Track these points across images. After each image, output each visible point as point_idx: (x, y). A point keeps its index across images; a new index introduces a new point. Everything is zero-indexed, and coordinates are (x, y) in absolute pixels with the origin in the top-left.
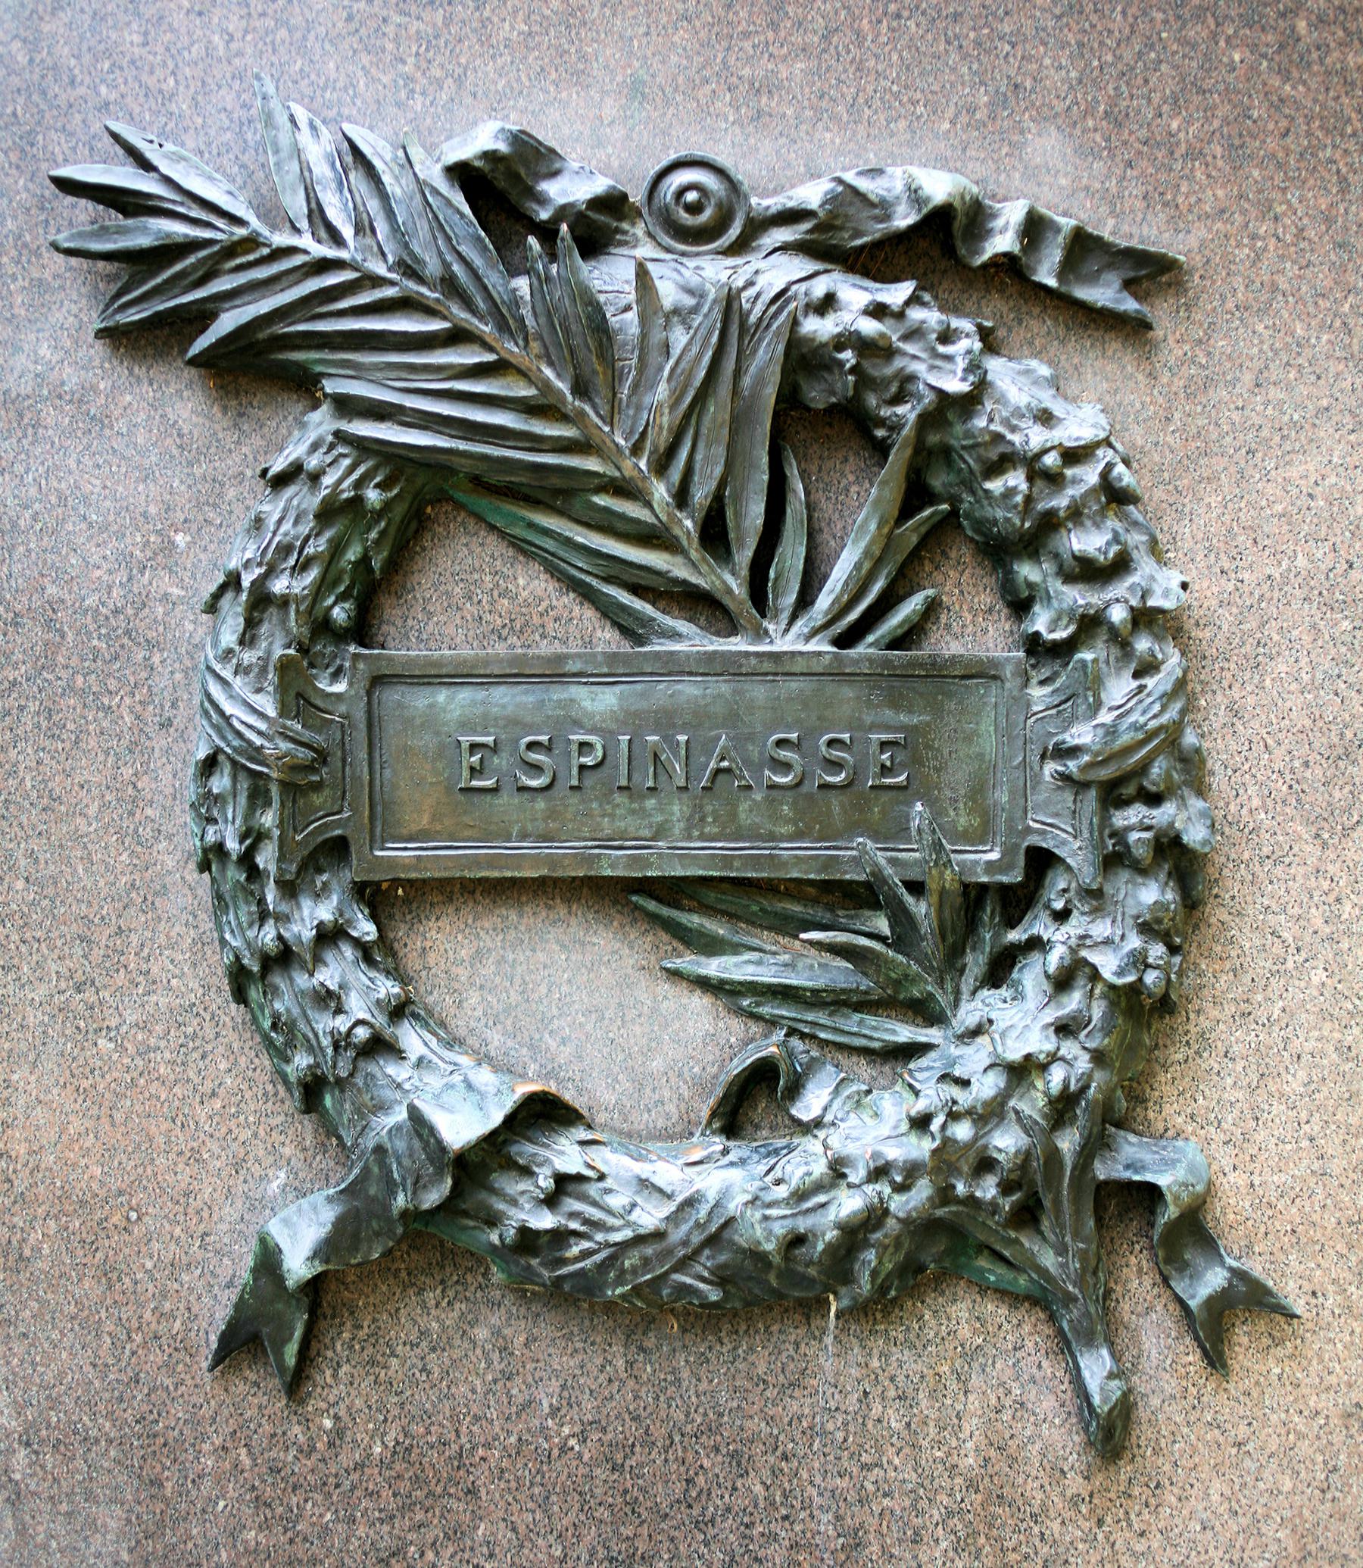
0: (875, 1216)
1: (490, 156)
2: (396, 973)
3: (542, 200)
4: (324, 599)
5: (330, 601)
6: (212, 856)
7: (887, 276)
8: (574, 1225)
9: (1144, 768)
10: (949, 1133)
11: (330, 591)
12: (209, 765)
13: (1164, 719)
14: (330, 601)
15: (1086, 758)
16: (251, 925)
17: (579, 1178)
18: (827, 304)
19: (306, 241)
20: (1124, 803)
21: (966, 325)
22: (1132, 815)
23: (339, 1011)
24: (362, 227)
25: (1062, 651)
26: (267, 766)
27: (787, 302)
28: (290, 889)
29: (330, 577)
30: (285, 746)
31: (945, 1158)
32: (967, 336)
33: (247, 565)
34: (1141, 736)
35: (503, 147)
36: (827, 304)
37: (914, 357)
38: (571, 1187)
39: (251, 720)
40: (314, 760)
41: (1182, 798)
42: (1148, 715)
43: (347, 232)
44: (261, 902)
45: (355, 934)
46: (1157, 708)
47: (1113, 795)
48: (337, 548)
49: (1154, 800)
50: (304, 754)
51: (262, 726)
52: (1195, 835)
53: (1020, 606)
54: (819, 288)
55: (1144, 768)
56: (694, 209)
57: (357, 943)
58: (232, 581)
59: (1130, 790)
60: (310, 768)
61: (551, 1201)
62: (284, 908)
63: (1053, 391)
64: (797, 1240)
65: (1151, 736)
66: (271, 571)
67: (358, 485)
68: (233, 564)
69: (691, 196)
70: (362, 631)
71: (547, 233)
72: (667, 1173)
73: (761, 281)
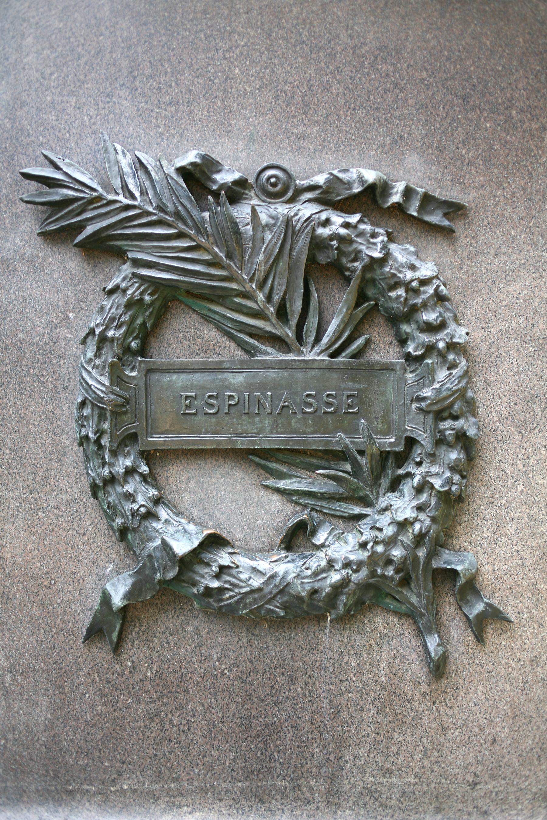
0: (345, 582)
1: (193, 164)
2: (156, 486)
3: (214, 182)
4: (128, 339)
5: (130, 340)
6: (84, 440)
7: (350, 212)
8: (227, 586)
9: (451, 405)
10: (374, 549)
11: (130, 335)
12: (83, 404)
13: (460, 386)
14: (130, 340)
15: (429, 402)
16: (99, 467)
17: (229, 567)
18: (327, 222)
19: (121, 198)
20: (444, 419)
21: (382, 231)
22: (447, 424)
23: (134, 501)
24: (143, 192)
25: (420, 359)
26: (106, 405)
27: (311, 222)
28: (114, 453)
29: (130, 330)
30: (112, 397)
31: (373, 558)
32: (382, 235)
33: (98, 325)
34: (450, 393)
35: (198, 160)
36: (327, 222)
37: (361, 244)
38: (225, 571)
39: (99, 386)
40: (124, 402)
41: (467, 417)
42: (453, 385)
43: (137, 194)
44: (103, 458)
45: (140, 471)
46: (457, 382)
47: (440, 416)
48: (133, 319)
49: (456, 418)
50: (120, 400)
51: (104, 389)
52: (472, 432)
53: (403, 341)
54: (323, 216)
55: (451, 405)
56: (274, 185)
57: (141, 474)
58: (92, 332)
59: (446, 414)
60: (122, 406)
61: (217, 576)
62: (112, 460)
63: (415, 257)
64: (315, 592)
65: (454, 393)
66: (107, 328)
67: (142, 294)
68: (92, 325)
69: (273, 180)
70: (143, 351)
71: (216, 195)
72: (263, 565)
73: (301, 214)
